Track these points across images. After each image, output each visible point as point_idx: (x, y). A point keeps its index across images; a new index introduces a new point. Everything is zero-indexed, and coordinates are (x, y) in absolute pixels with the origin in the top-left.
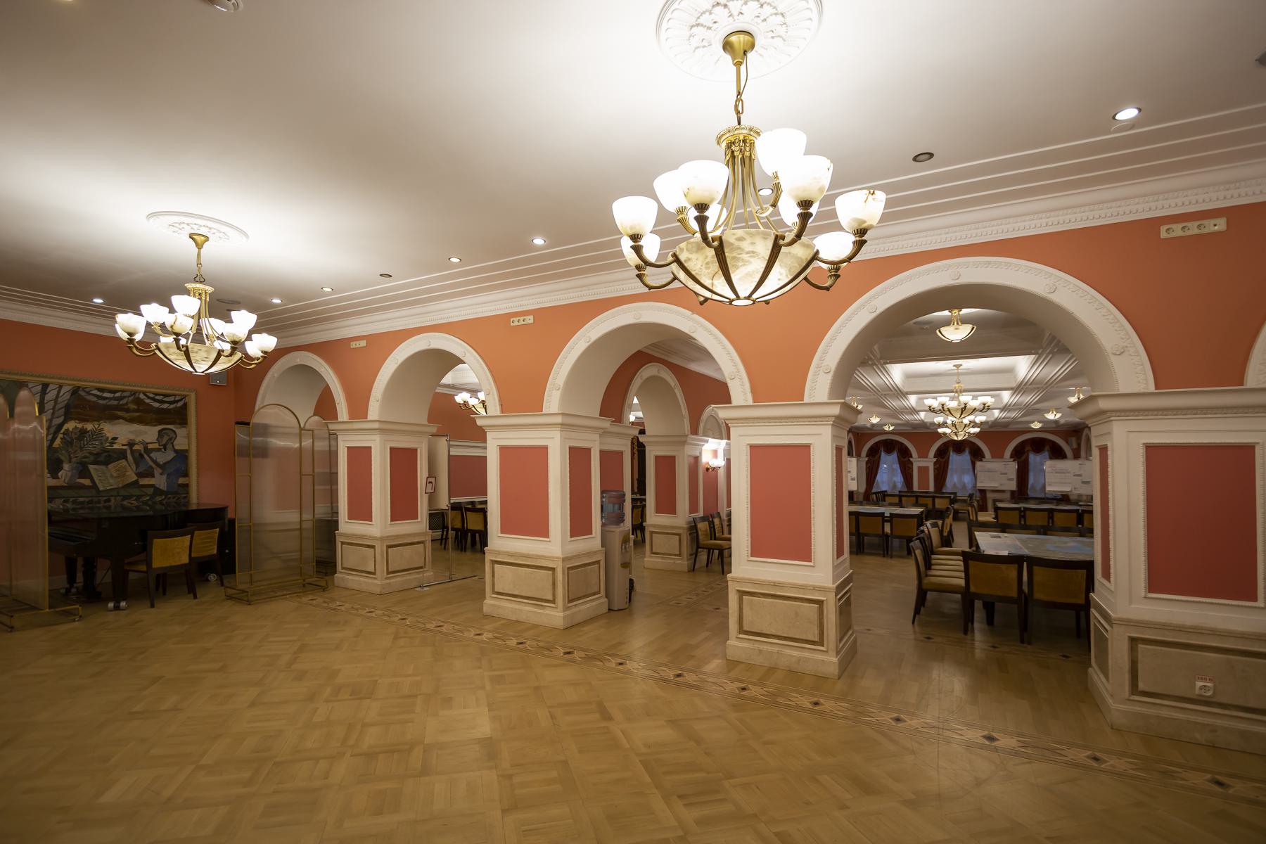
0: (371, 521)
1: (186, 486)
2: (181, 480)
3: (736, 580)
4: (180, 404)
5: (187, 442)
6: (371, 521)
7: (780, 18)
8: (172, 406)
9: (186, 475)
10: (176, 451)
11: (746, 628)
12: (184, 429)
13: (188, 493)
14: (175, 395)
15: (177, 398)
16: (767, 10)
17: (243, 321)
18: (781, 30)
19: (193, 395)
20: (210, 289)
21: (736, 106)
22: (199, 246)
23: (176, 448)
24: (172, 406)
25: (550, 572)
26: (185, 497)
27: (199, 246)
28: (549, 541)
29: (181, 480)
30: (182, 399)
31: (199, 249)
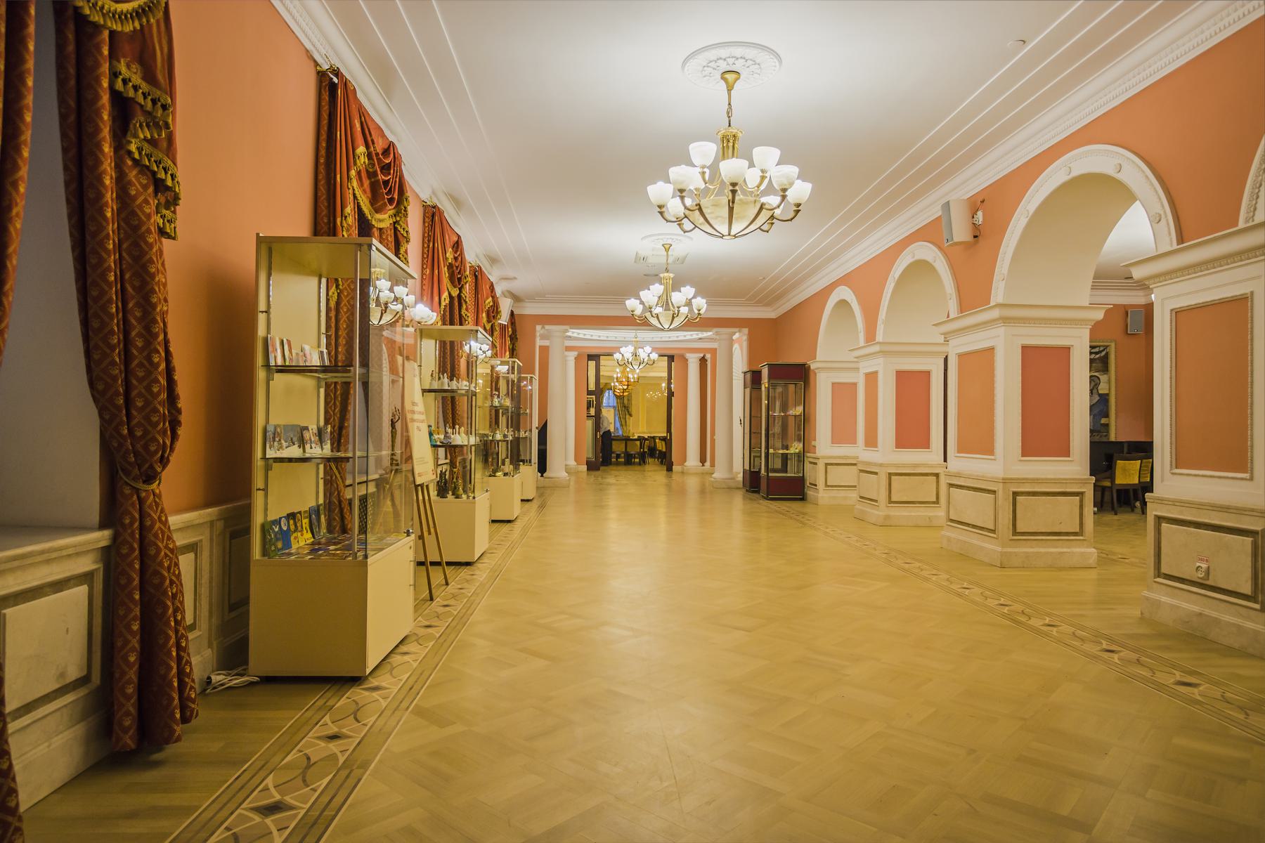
0: (876, 447)
1: (1107, 425)
2: (1104, 421)
3: (1161, 501)
4: (1103, 354)
5: (1108, 387)
6: (876, 447)
7: (757, 66)
8: (1098, 356)
9: (1107, 416)
10: (1100, 395)
11: (1164, 570)
12: (1105, 376)
13: (1108, 432)
14: (1099, 346)
15: (1102, 349)
16: (750, 62)
17: (688, 291)
18: (758, 71)
19: (1113, 345)
20: (672, 275)
21: (728, 113)
22: (667, 250)
23: (1100, 392)
24: (1098, 356)
25: (1078, 498)
26: (1106, 436)
27: (667, 250)
28: (995, 460)
29: (1104, 421)
30: (1104, 350)
31: (667, 252)
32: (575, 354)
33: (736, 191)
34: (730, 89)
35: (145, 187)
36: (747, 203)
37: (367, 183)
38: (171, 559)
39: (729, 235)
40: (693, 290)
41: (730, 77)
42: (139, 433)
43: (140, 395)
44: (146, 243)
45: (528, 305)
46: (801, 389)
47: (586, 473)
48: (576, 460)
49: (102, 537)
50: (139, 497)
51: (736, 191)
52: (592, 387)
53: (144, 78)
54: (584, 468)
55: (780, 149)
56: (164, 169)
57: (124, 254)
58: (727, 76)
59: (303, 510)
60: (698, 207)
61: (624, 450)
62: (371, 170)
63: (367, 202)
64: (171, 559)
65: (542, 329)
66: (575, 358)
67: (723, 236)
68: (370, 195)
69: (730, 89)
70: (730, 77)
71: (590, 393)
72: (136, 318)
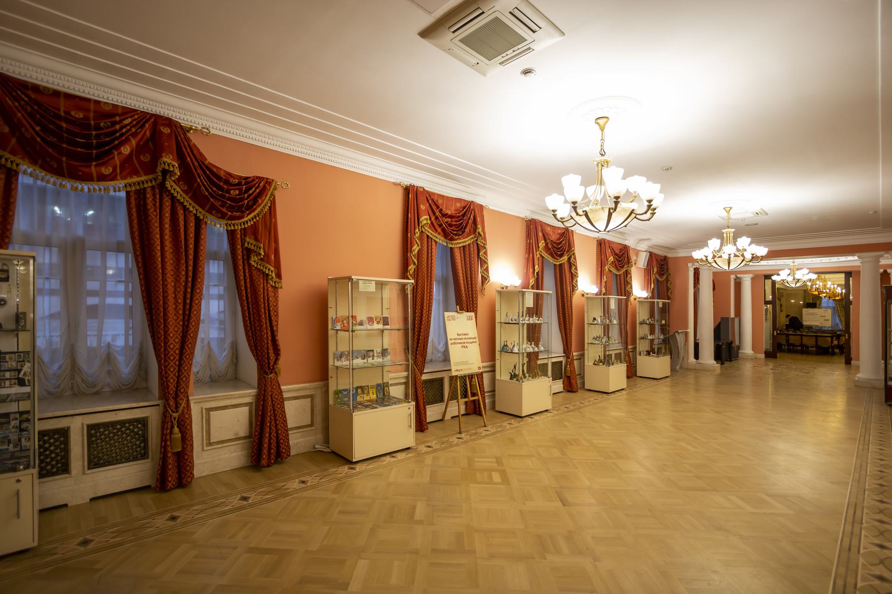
20: (733, 230)
27: (728, 212)
32: (751, 276)
33: (577, 207)
34: (602, 129)
35: (259, 276)
36: (596, 211)
37: (439, 230)
38: (281, 405)
39: (605, 231)
40: (749, 240)
41: (601, 121)
42: (260, 359)
43: (259, 346)
44: (259, 295)
45: (679, 251)
46: (617, 347)
47: (764, 360)
48: (753, 350)
49: (405, 374)
50: (265, 380)
51: (577, 207)
52: (769, 297)
53: (255, 240)
54: (763, 356)
55: (580, 175)
56: (266, 268)
57: (253, 299)
58: (599, 121)
59: (370, 384)
60: (584, 213)
61: (814, 343)
62: (439, 224)
63: (442, 238)
64: (281, 405)
65: (692, 265)
66: (752, 279)
67: (600, 231)
68: (442, 234)
69: (602, 129)
70: (601, 121)
71: (767, 303)
72: (257, 320)
